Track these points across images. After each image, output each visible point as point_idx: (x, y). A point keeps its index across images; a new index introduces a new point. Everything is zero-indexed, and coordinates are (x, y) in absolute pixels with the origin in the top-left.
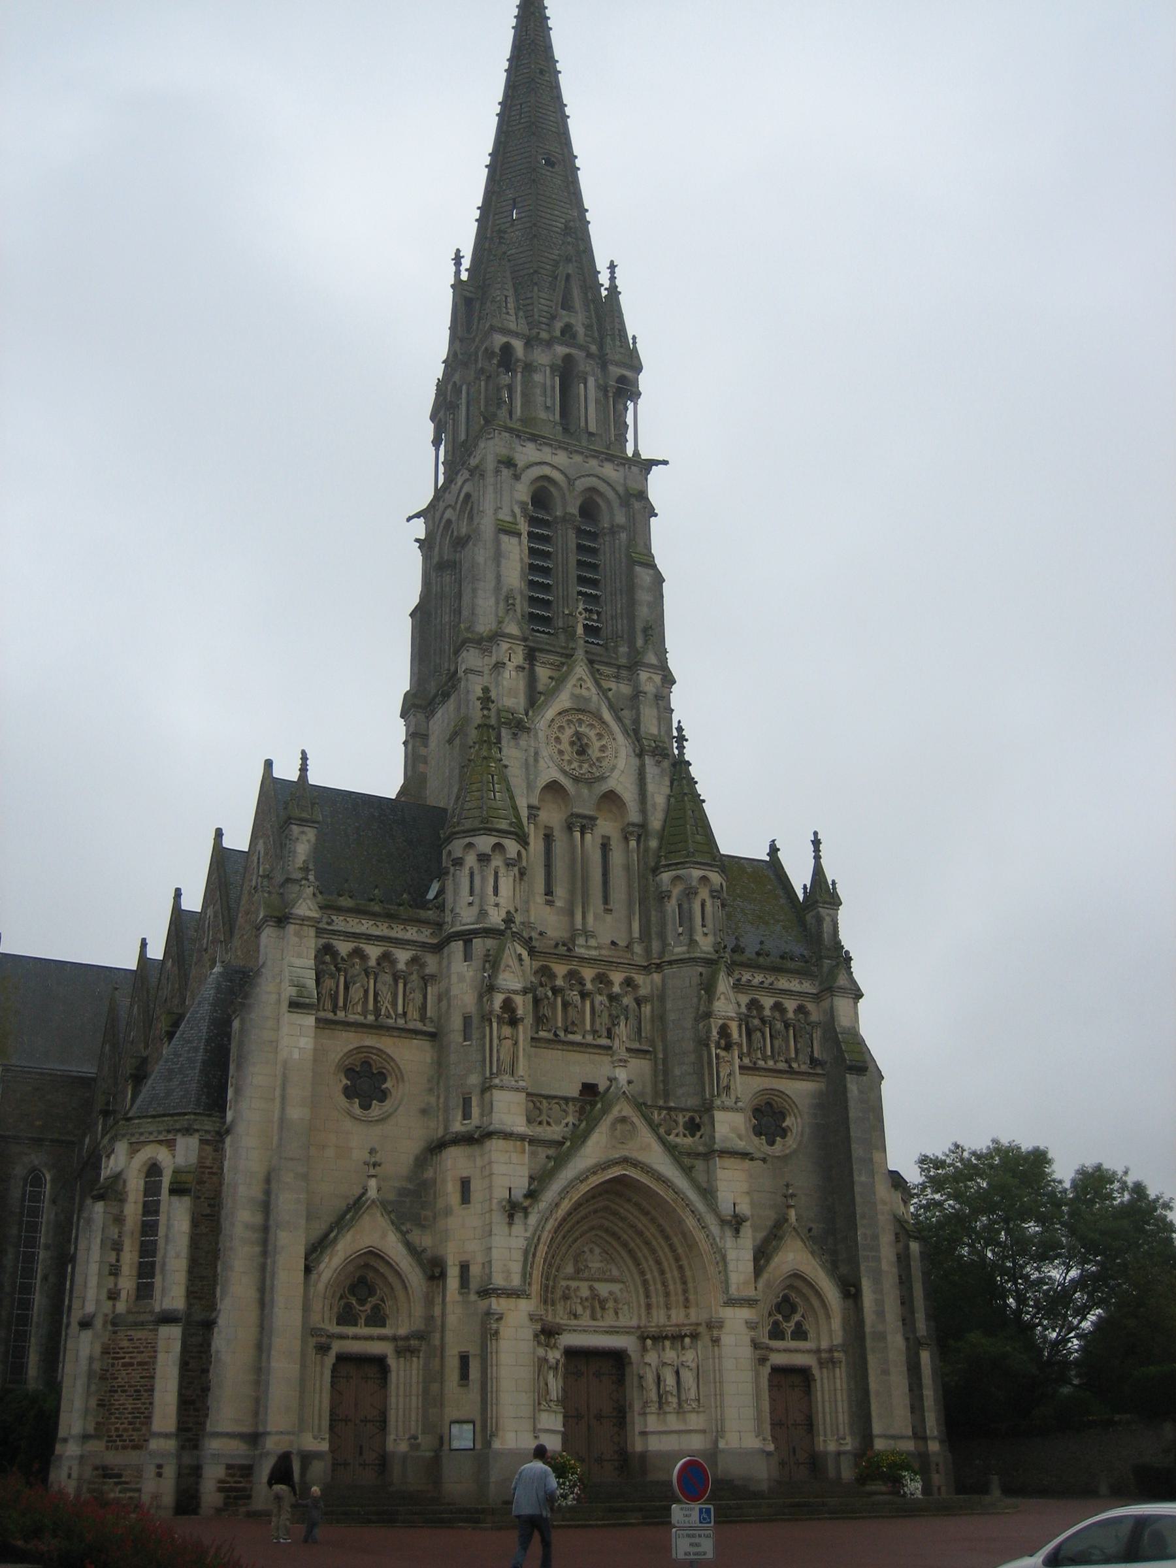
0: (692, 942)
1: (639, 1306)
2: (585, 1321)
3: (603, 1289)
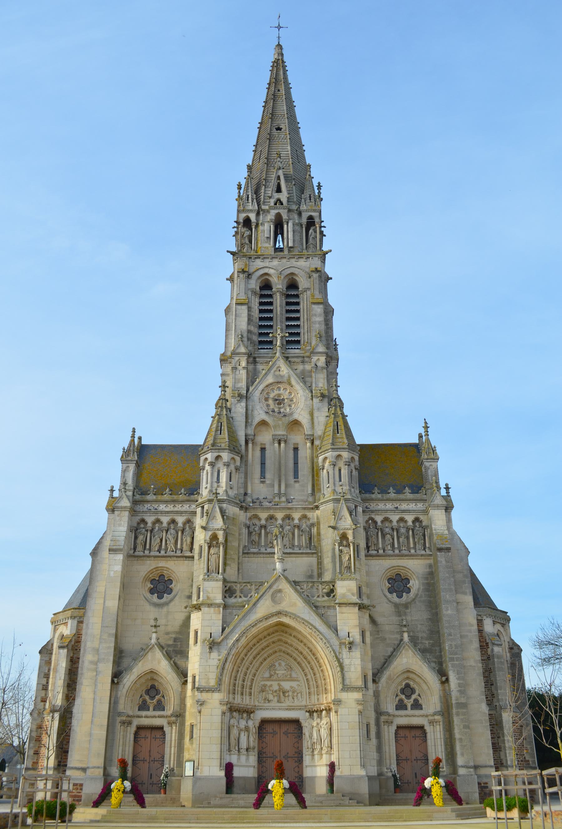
2: (274, 704)
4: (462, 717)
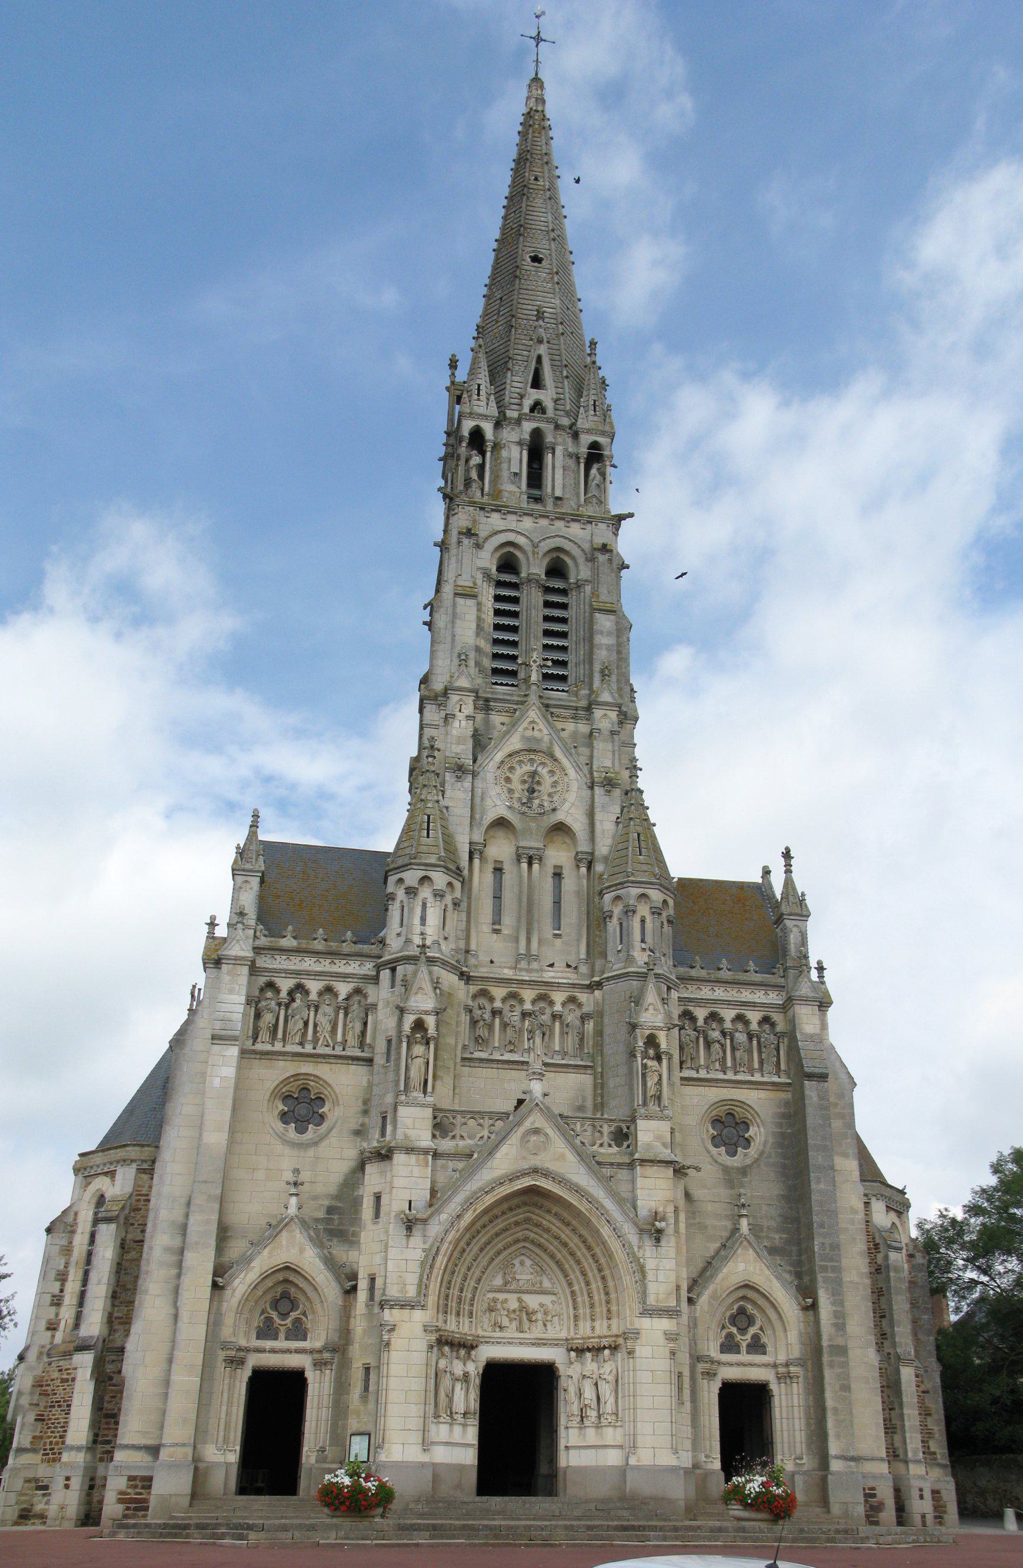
0: (630, 960)
1: (569, 1317)
2: (511, 1333)
3: (532, 1301)
4: (839, 1370)
